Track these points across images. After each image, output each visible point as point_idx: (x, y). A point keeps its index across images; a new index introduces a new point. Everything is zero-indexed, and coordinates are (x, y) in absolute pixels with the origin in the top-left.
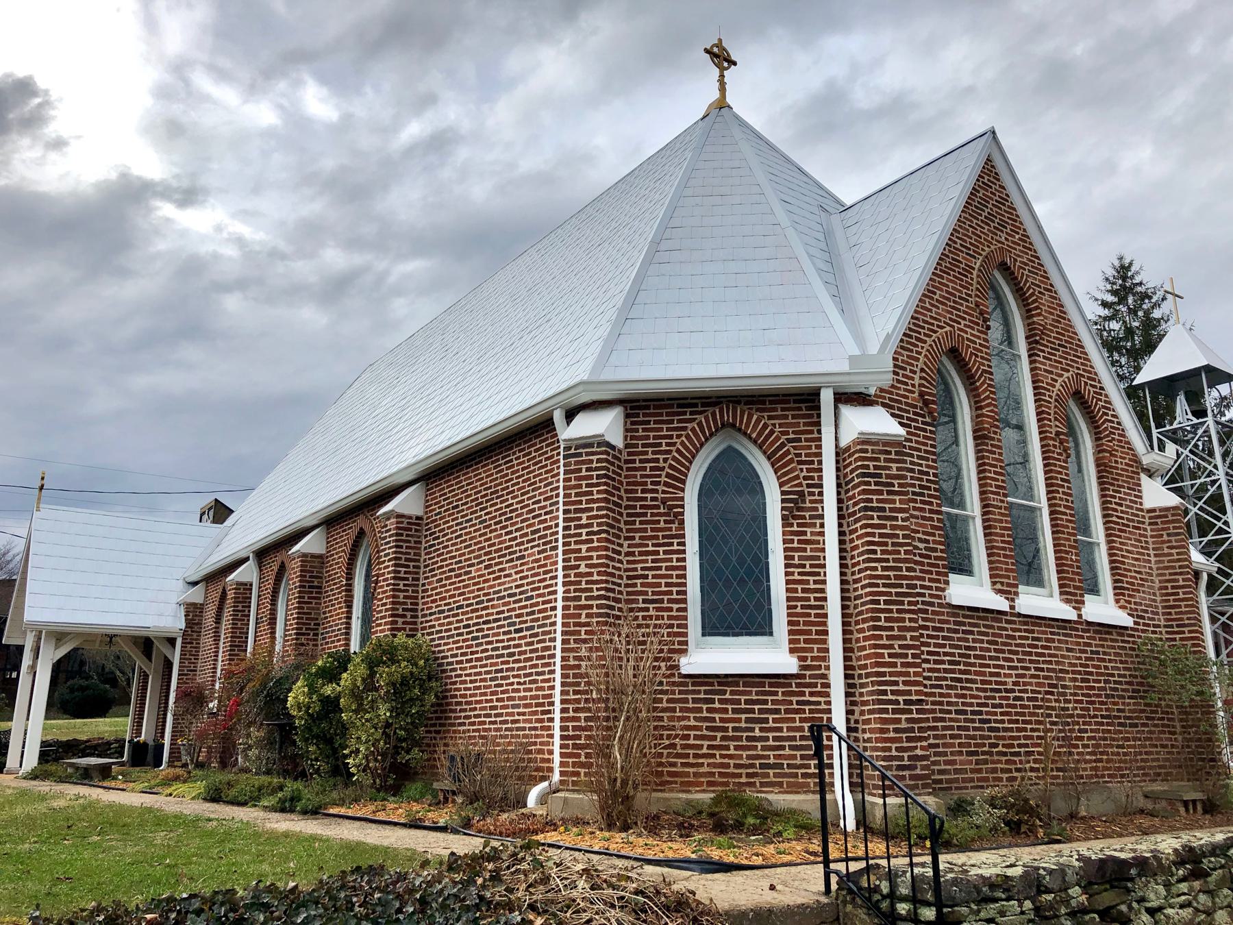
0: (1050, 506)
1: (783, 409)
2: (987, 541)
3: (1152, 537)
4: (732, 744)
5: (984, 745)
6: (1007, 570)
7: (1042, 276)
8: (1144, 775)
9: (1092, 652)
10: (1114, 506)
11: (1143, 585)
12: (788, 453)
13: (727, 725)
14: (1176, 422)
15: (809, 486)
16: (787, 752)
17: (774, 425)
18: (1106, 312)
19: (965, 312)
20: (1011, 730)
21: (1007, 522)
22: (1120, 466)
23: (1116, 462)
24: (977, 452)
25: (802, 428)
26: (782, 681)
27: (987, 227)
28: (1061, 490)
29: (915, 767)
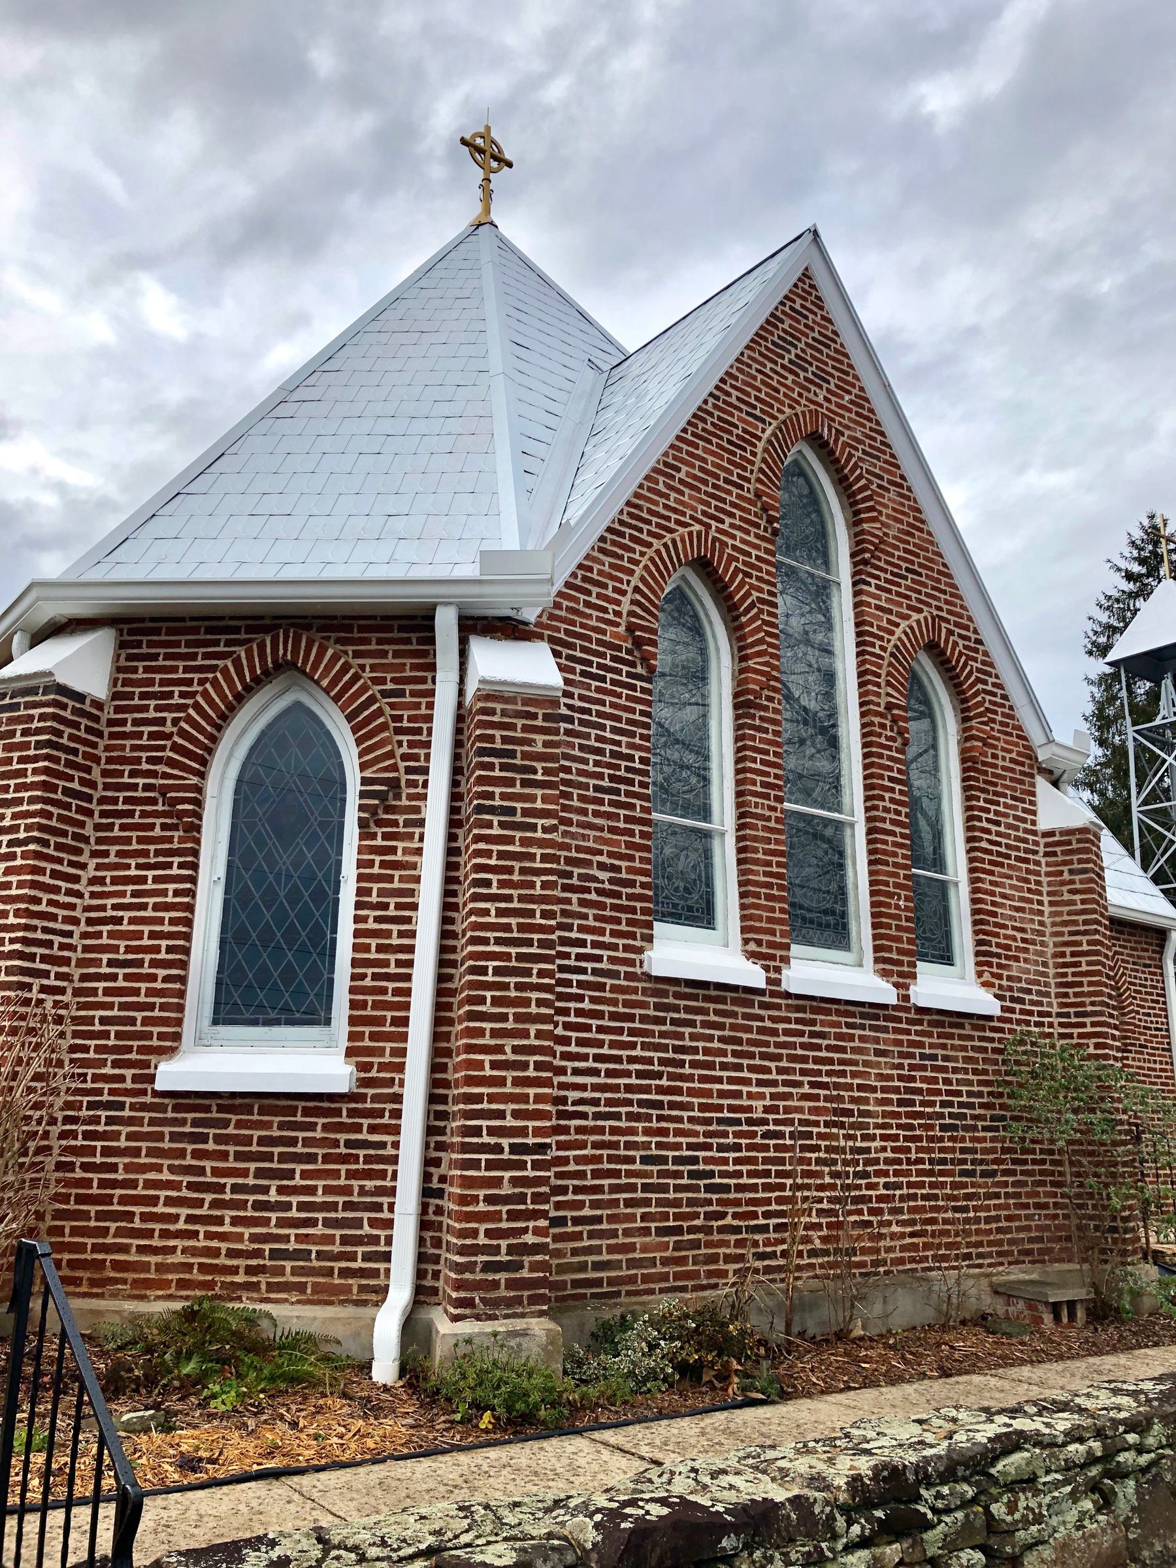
0: (869, 820)
1: (380, 642)
2: (742, 872)
3: (1048, 874)
4: (228, 1214)
5: (696, 1216)
6: (770, 920)
7: (886, 462)
8: (1000, 1254)
9: (923, 1057)
10: (985, 824)
11: (1026, 950)
12: (379, 712)
13: (223, 1181)
14: (1160, 717)
15: (409, 771)
16: (319, 1230)
17: (362, 667)
18: (1130, 587)
19: (733, 504)
20: (753, 1188)
21: (777, 842)
22: (1000, 763)
23: (994, 756)
24: (738, 728)
25: (408, 674)
26: (326, 1105)
27: (791, 377)
28: (887, 795)
29: (519, 1266)
